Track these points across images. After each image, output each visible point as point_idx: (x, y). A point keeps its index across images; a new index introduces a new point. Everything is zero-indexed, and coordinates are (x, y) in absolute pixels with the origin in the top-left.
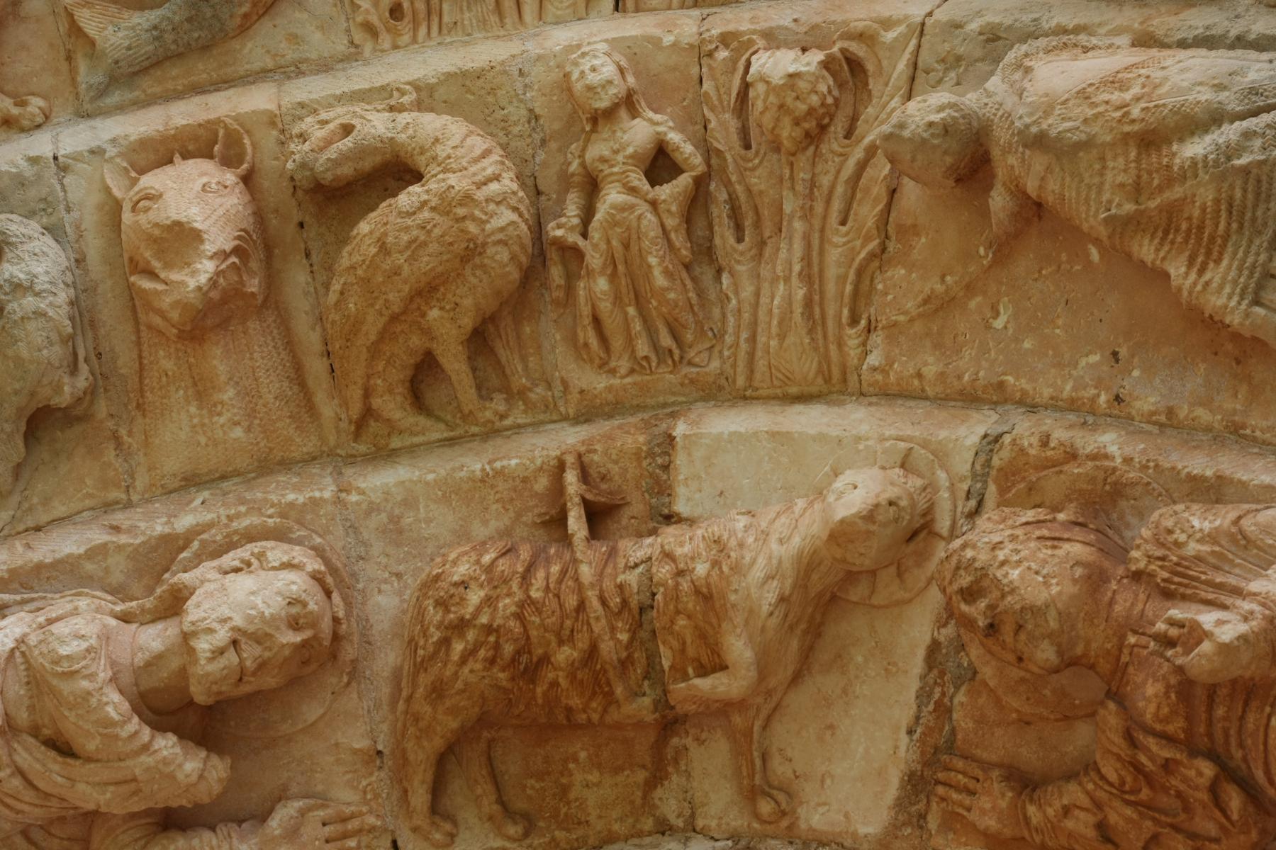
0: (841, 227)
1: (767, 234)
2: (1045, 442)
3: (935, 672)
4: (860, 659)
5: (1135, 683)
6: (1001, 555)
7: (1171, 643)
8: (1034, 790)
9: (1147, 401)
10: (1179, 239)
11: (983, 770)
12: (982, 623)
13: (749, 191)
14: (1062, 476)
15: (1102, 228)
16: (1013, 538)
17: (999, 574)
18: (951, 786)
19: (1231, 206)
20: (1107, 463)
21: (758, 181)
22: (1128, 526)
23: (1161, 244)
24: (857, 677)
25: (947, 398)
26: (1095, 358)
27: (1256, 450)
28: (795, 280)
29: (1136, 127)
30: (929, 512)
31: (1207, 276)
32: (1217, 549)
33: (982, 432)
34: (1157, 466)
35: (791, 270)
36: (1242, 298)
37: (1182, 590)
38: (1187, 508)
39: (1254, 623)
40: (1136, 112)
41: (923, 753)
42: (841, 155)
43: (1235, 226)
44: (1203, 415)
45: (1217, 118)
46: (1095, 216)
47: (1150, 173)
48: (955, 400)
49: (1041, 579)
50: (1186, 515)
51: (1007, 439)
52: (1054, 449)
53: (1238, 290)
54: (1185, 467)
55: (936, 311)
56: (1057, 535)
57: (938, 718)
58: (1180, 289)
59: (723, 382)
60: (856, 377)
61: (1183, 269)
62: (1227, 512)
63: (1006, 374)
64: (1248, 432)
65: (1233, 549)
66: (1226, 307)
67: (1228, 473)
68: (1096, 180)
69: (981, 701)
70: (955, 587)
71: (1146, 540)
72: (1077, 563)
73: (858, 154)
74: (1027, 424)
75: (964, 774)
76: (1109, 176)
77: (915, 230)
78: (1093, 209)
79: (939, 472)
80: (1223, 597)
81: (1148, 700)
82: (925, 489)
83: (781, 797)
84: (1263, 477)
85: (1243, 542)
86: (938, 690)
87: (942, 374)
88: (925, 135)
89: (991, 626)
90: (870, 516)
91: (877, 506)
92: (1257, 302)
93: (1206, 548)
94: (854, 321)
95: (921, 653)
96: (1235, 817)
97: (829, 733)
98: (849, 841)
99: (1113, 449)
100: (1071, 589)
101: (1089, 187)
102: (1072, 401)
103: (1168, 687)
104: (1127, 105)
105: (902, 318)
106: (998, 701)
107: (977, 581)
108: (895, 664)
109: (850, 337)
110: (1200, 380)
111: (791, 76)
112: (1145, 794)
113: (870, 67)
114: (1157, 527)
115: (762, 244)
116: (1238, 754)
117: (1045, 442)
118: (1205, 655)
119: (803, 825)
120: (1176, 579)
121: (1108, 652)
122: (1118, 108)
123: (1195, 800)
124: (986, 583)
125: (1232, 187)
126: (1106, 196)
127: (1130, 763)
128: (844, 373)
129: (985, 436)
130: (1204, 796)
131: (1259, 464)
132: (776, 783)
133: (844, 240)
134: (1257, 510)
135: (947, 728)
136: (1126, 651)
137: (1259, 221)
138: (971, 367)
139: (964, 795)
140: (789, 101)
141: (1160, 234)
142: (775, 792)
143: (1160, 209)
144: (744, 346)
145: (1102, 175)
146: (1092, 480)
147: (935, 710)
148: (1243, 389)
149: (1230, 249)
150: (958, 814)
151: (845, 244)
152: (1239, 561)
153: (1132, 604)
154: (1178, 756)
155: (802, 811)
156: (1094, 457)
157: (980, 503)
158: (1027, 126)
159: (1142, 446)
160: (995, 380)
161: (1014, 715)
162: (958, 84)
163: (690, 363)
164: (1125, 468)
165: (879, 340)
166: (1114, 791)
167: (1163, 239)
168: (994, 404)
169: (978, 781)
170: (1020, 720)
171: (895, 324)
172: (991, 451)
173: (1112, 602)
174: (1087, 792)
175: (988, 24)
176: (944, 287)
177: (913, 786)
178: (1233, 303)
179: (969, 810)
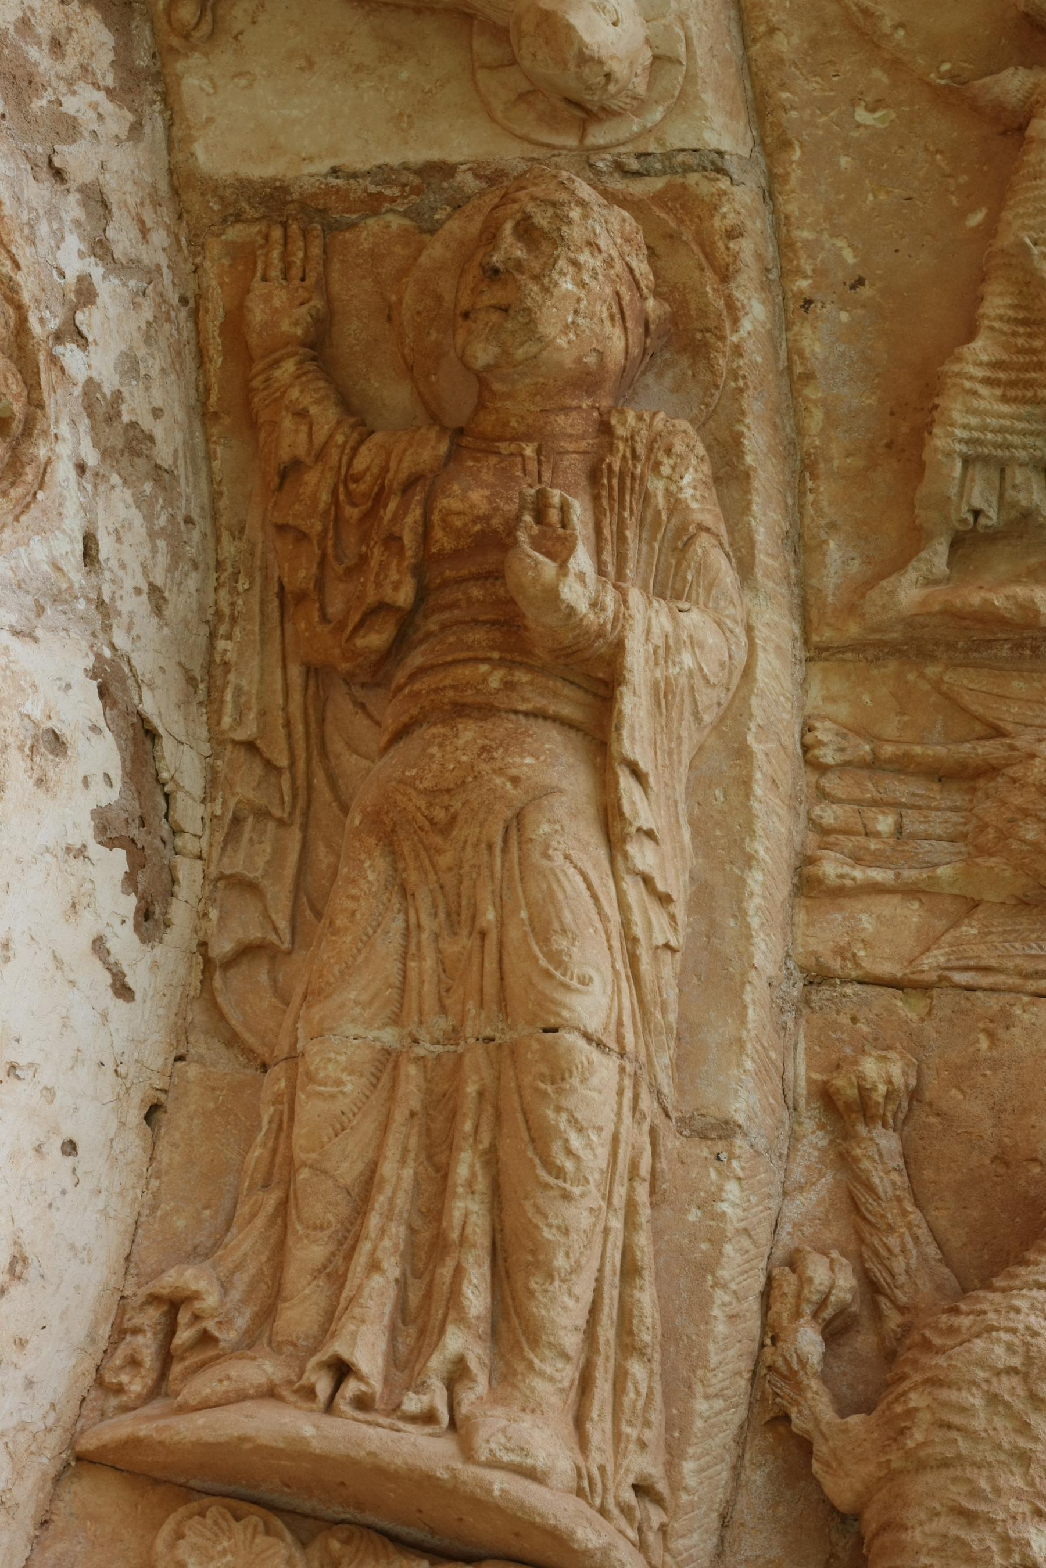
2: (732, 234)
3: (416, 181)
4: (404, 75)
5: (479, 470)
6: (584, 257)
7: (540, 517)
8: (314, 359)
10: (1020, 341)
11: (317, 281)
12: (496, 259)
14: (697, 273)
15: (1012, 239)
16: (609, 263)
17: (562, 263)
18: (285, 244)
20: (728, 325)
22: (660, 375)
23: (1009, 320)
24: (381, 78)
25: (753, 76)
27: (790, 501)
30: (607, 113)
31: (984, 391)
32: (664, 517)
33: (723, 148)
34: (741, 391)
36: (968, 442)
37: (604, 493)
38: (702, 459)
39: (592, 616)
41: (314, 196)
44: (815, 421)
46: (1024, 227)
48: (753, 86)
49: (570, 320)
50: (694, 462)
51: (724, 184)
52: (728, 249)
53: (976, 434)
54: (749, 428)
55: (857, 28)
56: (628, 313)
57: (362, 202)
58: (960, 359)
61: (985, 358)
62: (709, 511)
64: (810, 484)
65: (669, 535)
66: (952, 425)
67: (756, 484)
69: (398, 249)
70: (531, 208)
71: (650, 425)
72: (601, 354)
74: (748, 199)
75: (306, 257)
78: (1032, 222)
79: (661, 109)
80: (609, 547)
81: (464, 498)
82: (635, 98)
83: (205, 28)
84: (761, 530)
85: (680, 544)
86: (395, 191)
87: (782, 61)
89: (496, 271)
90: (585, 59)
91: (601, 63)
92: (967, 461)
93: (661, 501)
95: (434, 155)
96: (360, 642)
97: (303, 63)
98: (180, 134)
99: (747, 325)
100: (568, 362)
103: (486, 518)
106: (403, 272)
107: (544, 235)
108: (411, 125)
110: (855, 402)
112: (352, 513)
114: (669, 433)
116: (432, 624)
117: (732, 234)
118: (539, 574)
119: (180, 66)
120: (615, 482)
121: (506, 424)
123: (364, 585)
124: (546, 247)
127: (382, 488)
129: (720, 154)
130: (371, 598)
131: (775, 515)
132: (220, 12)
134: (721, 545)
135: (354, 216)
136: (513, 447)
138: (798, 95)
139: (280, 265)
141: (1021, 315)
142: (209, 17)
146: (703, 313)
147: (370, 195)
148: (856, 462)
149: (1024, 410)
150: (255, 263)
152: (657, 546)
153: (571, 436)
154: (409, 553)
155: (196, 59)
156: (731, 304)
157: (637, 174)
159: (759, 359)
160: (791, 135)
161: (394, 298)
166: (343, 471)
167: (1016, 321)
168: (761, 142)
169: (303, 279)
170: (390, 307)
172: (705, 169)
173: (565, 409)
174: (331, 436)
176: (888, 31)
177: (272, 196)
178: (958, 432)
179: (265, 279)
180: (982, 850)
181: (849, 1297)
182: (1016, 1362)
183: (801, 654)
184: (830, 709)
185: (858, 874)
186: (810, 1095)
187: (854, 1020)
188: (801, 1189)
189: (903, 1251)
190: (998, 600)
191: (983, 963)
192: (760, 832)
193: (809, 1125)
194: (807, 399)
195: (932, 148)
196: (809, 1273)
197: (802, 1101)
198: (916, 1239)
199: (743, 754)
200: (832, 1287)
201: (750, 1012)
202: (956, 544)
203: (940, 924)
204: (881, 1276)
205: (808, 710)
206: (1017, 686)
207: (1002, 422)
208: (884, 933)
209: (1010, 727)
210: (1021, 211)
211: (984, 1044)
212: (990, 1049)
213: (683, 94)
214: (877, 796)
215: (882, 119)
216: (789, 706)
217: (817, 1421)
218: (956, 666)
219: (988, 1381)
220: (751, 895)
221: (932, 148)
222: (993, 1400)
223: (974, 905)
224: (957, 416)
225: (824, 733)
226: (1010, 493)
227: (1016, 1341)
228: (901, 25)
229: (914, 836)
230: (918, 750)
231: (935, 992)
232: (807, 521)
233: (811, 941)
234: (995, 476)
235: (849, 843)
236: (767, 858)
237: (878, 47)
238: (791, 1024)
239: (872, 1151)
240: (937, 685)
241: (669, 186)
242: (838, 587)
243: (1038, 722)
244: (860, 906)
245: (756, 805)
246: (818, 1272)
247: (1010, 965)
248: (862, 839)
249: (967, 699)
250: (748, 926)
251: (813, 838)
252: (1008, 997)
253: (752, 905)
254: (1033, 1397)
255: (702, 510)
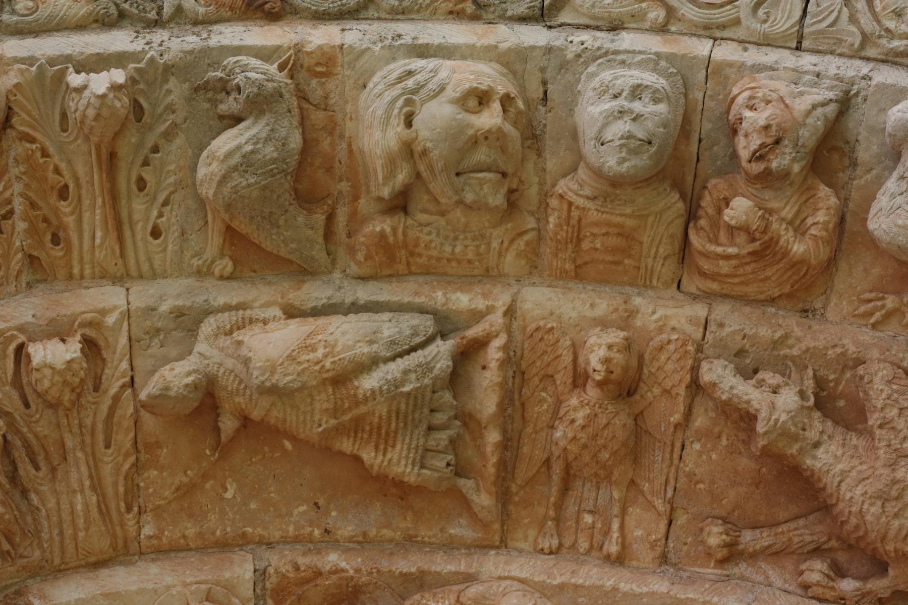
0: (107, 451)
1: (56, 463)
2: (297, 568)
9: (347, 529)
10: (365, 436)
13: (36, 436)
19: (398, 413)
20: (344, 574)
21: (42, 429)
26: (303, 508)
28: (87, 491)
29: (330, 374)
31: (389, 456)
34: (378, 571)
35: (83, 485)
36: (413, 465)
38: (423, 597)
40: (328, 365)
42: (95, 403)
43: (401, 425)
44: (387, 533)
45: (375, 362)
47: (342, 400)
50: (424, 601)
51: (271, 570)
52: (305, 571)
53: (410, 462)
58: (372, 466)
59: (44, 563)
60: (137, 544)
61: (373, 454)
63: (245, 527)
64: (419, 539)
66: (404, 472)
67: (426, 567)
68: (309, 408)
73: (107, 402)
76: (317, 405)
77: (158, 444)
87: (200, 533)
88: (185, 393)
94: (129, 509)
99: (343, 564)
101: (305, 413)
102: (296, 537)
104: (321, 362)
105: (162, 502)
109: (129, 520)
111: (69, 362)
113: (102, 343)
115: (53, 470)
122: (317, 363)
125: (399, 403)
126: (316, 418)
128: (125, 542)
133: (111, 458)
137: (417, 420)
138: (216, 525)
140: (69, 378)
141: (352, 434)
143: (351, 420)
144: (57, 539)
145: (311, 405)
148: (410, 515)
149: (400, 438)
151: (112, 461)
156: (335, 572)
158: (263, 382)
160: (240, 532)
162: (162, 347)
163: (21, 557)
164: (358, 575)
165: (149, 519)
167: (355, 437)
171: (159, 507)
175: (175, 306)
178: (409, 470)
180: (608, 477)
181: (825, 564)
182: (879, 503)
183: (504, 551)
184: (531, 539)
185: (615, 535)
186: (721, 568)
187: (685, 544)
188: (767, 577)
189: (801, 535)
190: (494, 460)
191: (664, 482)
192: (601, 582)
193: (736, 570)
194: (376, 536)
195: (249, 462)
196: (814, 581)
197: (724, 572)
198: (796, 529)
199: (562, 587)
200: (821, 572)
201: (690, 596)
202: (457, 474)
203: (641, 499)
204: (812, 546)
205: (531, 550)
206: (526, 450)
207: (405, 448)
208: (644, 526)
209: (546, 456)
210: (301, 430)
211: (701, 486)
212: (704, 484)
213: (224, 587)
214: (574, 521)
215: (231, 485)
216: (533, 561)
217: (888, 587)
218: (513, 478)
219: (887, 517)
220: (632, 590)
221: (249, 462)
222: (896, 516)
223: (632, 482)
224: (400, 470)
225: (545, 544)
226: (440, 448)
227: (869, 501)
228: (185, 472)
229: (595, 505)
230: (552, 499)
231: (675, 505)
232: (438, 542)
233: (647, 560)
234: (431, 454)
235: (598, 538)
236: (613, 580)
237: (195, 484)
238: (687, 574)
239: (752, 544)
240: (522, 487)
241: (272, 597)
242: (474, 531)
243: (544, 442)
244: (630, 535)
245: (587, 583)
246: (815, 577)
247: (666, 470)
248: (596, 531)
249: (530, 474)
250: (647, 593)
251: (595, 553)
252: (681, 474)
253: (637, 590)
254: (897, 499)
255: (449, 599)
